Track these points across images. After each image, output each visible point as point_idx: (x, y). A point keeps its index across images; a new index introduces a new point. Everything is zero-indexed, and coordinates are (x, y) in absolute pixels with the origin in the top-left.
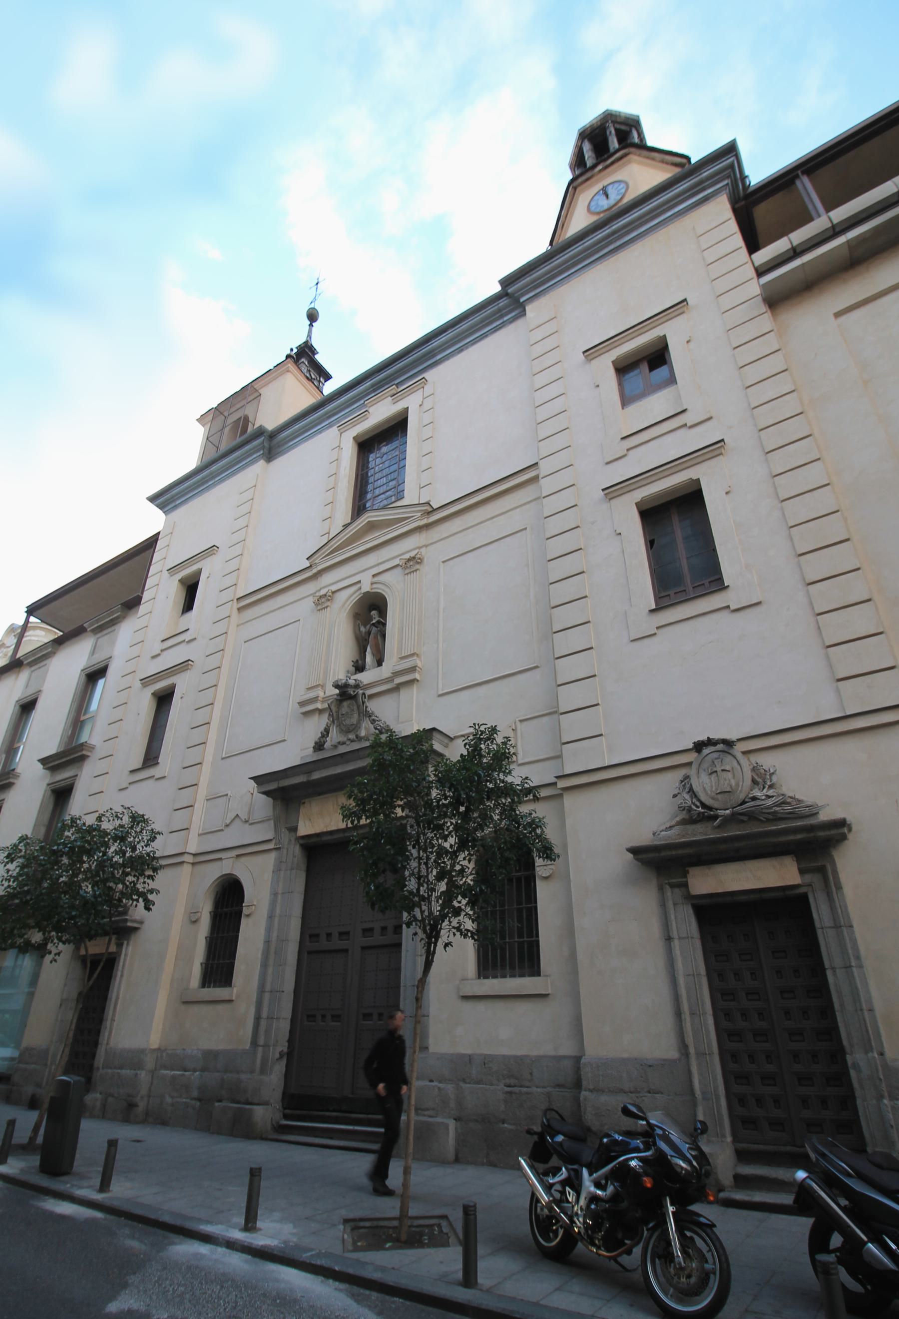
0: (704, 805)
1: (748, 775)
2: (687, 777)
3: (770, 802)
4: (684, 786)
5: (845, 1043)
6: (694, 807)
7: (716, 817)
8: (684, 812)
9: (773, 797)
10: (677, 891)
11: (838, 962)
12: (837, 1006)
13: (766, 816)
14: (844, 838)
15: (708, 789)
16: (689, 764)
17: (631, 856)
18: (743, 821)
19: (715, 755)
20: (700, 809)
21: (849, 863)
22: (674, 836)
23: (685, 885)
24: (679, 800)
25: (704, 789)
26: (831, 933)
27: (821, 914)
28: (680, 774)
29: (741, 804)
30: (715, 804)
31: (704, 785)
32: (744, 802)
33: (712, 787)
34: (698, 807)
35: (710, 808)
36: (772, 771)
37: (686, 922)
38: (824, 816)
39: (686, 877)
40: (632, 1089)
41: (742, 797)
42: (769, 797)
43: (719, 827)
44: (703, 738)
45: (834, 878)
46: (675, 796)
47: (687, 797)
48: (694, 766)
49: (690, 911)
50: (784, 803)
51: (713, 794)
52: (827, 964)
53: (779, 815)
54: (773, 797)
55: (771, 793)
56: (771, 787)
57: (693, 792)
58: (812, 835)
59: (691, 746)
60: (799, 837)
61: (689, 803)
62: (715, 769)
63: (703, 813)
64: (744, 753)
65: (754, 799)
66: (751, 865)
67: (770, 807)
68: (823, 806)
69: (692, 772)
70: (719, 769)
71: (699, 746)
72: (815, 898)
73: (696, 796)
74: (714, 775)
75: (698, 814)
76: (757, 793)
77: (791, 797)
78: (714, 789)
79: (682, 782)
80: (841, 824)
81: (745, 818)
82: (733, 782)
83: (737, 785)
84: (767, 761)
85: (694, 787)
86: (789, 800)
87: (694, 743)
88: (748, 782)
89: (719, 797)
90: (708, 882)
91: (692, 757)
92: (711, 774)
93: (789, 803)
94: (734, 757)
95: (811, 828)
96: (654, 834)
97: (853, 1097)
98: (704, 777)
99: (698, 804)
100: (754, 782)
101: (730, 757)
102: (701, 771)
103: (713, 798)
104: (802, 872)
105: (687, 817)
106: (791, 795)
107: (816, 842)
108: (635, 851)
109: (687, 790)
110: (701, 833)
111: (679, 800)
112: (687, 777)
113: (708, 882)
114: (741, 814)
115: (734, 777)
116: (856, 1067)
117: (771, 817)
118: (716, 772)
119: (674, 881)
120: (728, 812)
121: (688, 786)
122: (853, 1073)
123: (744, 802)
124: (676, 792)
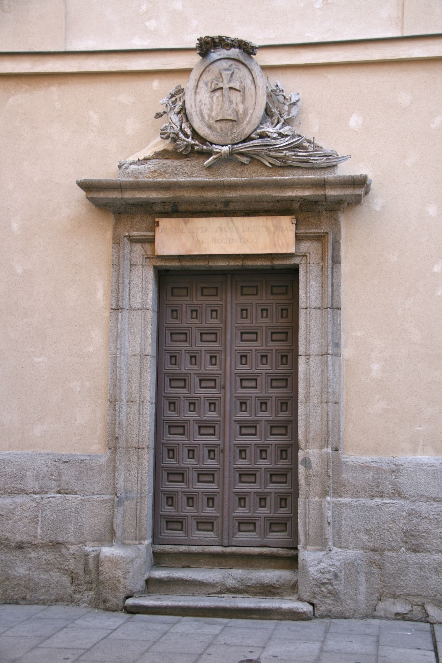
0: (195, 134)
1: (262, 101)
2: (180, 91)
3: (282, 142)
4: (174, 103)
5: (301, 437)
6: (181, 135)
7: (209, 154)
8: (168, 141)
9: (287, 136)
10: (138, 248)
11: (318, 198)
12: (301, 397)
13: (272, 161)
14: (357, 201)
15: (206, 112)
16: (187, 71)
17: (82, 193)
18: (243, 164)
19: (225, 64)
20: (190, 140)
21: (355, 237)
22: (147, 173)
23: (152, 241)
24: (163, 123)
25: (201, 111)
26: (315, 362)
27: (309, 290)
28: (171, 85)
29: (244, 141)
30: (211, 138)
31: (203, 106)
32: (249, 139)
33: (211, 110)
34: (187, 136)
35: (203, 140)
36: (293, 100)
37: (143, 288)
38: (345, 170)
39: (153, 230)
40: (37, 490)
41: (248, 130)
42: (282, 135)
43: (209, 167)
44: (214, 33)
45: (333, 249)
46: (159, 116)
47: (175, 119)
48: (194, 76)
49: (151, 275)
50: (299, 147)
51: (212, 121)
52: (301, 350)
53: (290, 163)
54: (287, 136)
55: (285, 130)
56: (286, 123)
57: (185, 114)
58: (320, 192)
59: (194, 44)
60: (307, 193)
61: (177, 129)
62: (221, 85)
63: (193, 146)
64: (264, 68)
65: (262, 136)
66: (240, 222)
67: (280, 150)
68: (345, 158)
69: (188, 84)
70: (226, 86)
71: (207, 46)
72: (306, 272)
73: (187, 120)
74: (218, 94)
75: (187, 147)
76: (269, 129)
77: (309, 141)
78: (214, 114)
79: (172, 96)
80: (361, 183)
81: (244, 160)
82: (241, 108)
83: (245, 112)
84: (292, 86)
85: (188, 106)
86: (306, 144)
87: (200, 40)
88: (260, 112)
89: (218, 126)
90: (178, 239)
91: (192, 61)
92: (214, 91)
93: (305, 148)
94: (250, 71)
95: (322, 184)
96: (120, 167)
97: (295, 494)
98: (204, 94)
99: (189, 132)
100: (268, 112)
101: (244, 70)
102: (201, 84)
103: (210, 127)
104: (299, 238)
105: (171, 148)
106: (310, 138)
107: (325, 204)
108: (87, 186)
109: (177, 109)
110: (190, 173)
111: (163, 123)
112: (180, 91)
113: (178, 239)
114: (242, 154)
115: (243, 101)
116: (307, 463)
117: (278, 163)
118: (222, 88)
119: (136, 234)
120: (226, 149)
121: (179, 104)
122: (301, 469)
123: (249, 139)
124: (161, 111)
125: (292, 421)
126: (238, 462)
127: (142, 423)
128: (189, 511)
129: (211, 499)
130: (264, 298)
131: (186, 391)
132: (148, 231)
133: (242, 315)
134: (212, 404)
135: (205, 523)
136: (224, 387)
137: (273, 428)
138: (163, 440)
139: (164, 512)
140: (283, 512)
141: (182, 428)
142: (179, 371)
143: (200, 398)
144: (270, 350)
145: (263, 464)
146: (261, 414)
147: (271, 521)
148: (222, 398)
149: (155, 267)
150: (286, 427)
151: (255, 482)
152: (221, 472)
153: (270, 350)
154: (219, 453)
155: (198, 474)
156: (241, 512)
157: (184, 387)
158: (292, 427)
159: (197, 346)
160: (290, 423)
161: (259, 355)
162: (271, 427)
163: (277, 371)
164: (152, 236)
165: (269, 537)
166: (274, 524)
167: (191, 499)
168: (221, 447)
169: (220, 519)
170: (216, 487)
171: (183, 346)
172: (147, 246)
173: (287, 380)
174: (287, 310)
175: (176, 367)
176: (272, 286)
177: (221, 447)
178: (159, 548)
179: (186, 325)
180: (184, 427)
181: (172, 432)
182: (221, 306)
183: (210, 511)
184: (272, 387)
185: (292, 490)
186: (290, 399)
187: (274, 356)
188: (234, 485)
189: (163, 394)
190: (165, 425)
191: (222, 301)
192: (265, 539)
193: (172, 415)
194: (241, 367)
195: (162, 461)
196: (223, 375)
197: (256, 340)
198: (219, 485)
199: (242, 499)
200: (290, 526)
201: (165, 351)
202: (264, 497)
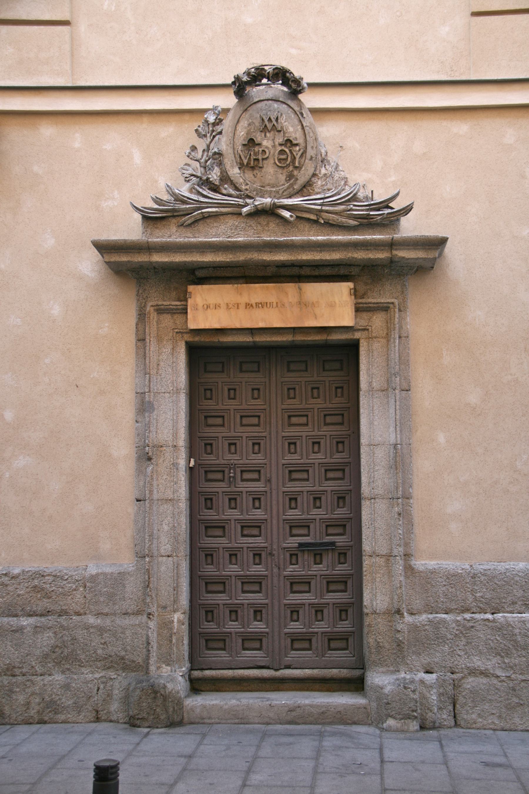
37: (174, 369)
59: (229, 80)
90: (214, 309)
113: (214, 309)
125: (350, 491)
126: (289, 654)
127: (173, 520)
128: (233, 569)
129: (256, 499)
130: (315, 375)
131: (226, 596)
132: (179, 300)
133: (289, 394)
134: (257, 555)
135: (251, 641)
136: (269, 481)
137: (328, 472)
138: (200, 571)
139: (204, 628)
140: (341, 513)
141: (222, 585)
142: (217, 462)
143: (242, 437)
144: (327, 604)
145: (317, 513)
146: (315, 511)
147: (328, 524)
148: (269, 605)
149: (187, 343)
150: (346, 582)
151: (309, 592)
152: (270, 581)
153: (327, 604)
154: (267, 555)
155: (243, 640)
156: (295, 627)
157: (223, 592)
158: (351, 497)
159: (237, 431)
160: (350, 578)
161: (310, 442)
162: (327, 526)
163: (332, 461)
164: (185, 305)
165: (326, 598)
166: (333, 640)
167: (234, 612)
168: (269, 548)
169: (268, 466)
170: (265, 627)
171: (221, 599)
172: (179, 318)
173: (344, 470)
174: (342, 388)
175: (212, 457)
176: (324, 361)
177: (269, 548)
178: (197, 674)
179: (223, 462)
180: (224, 527)
181: (210, 533)
182: (264, 383)
183: (258, 627)
184: (326, 424)
185: (352, 543)
186: (349, 521)
187: (328, 442)
188: (285, 597)
189: (199, 544)
190: (202, 526)
191: (265, 377)
192: (323, 658)
193: (211, 627)
194: (288, 457)
195: (199, 540)
196: (269, 576)
197: (307, 425)
198: (267, 624)
199: (295, 612)
200: (352, 613)
201: (199, 437)
202: (320, 609)
